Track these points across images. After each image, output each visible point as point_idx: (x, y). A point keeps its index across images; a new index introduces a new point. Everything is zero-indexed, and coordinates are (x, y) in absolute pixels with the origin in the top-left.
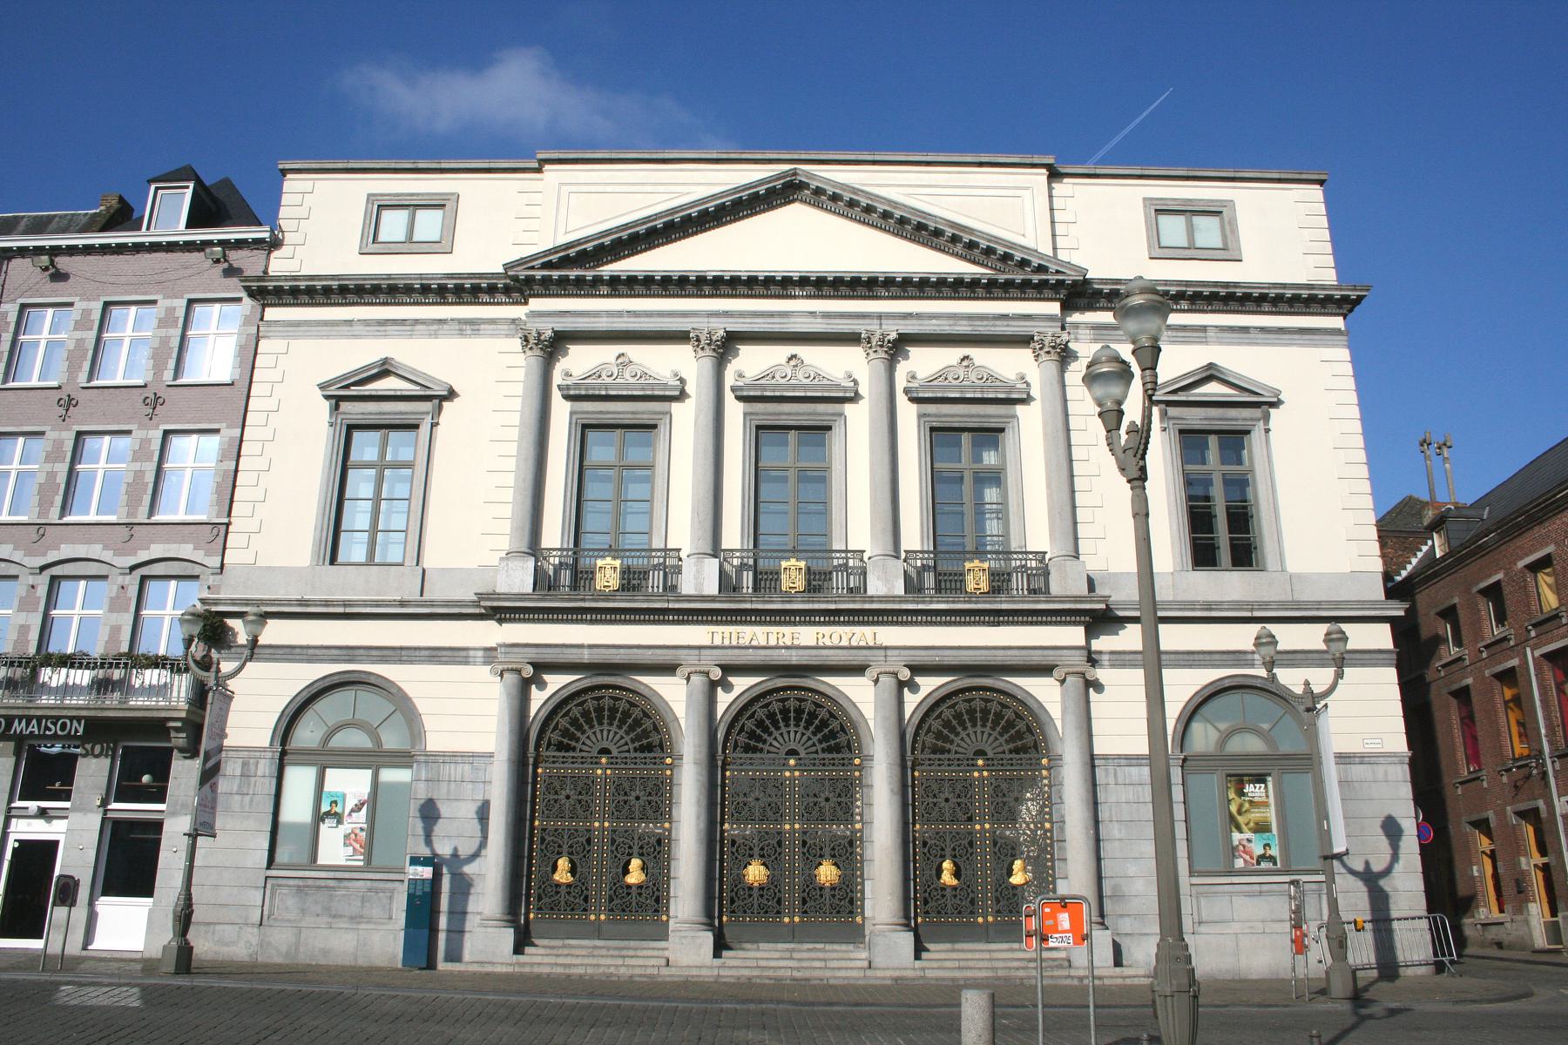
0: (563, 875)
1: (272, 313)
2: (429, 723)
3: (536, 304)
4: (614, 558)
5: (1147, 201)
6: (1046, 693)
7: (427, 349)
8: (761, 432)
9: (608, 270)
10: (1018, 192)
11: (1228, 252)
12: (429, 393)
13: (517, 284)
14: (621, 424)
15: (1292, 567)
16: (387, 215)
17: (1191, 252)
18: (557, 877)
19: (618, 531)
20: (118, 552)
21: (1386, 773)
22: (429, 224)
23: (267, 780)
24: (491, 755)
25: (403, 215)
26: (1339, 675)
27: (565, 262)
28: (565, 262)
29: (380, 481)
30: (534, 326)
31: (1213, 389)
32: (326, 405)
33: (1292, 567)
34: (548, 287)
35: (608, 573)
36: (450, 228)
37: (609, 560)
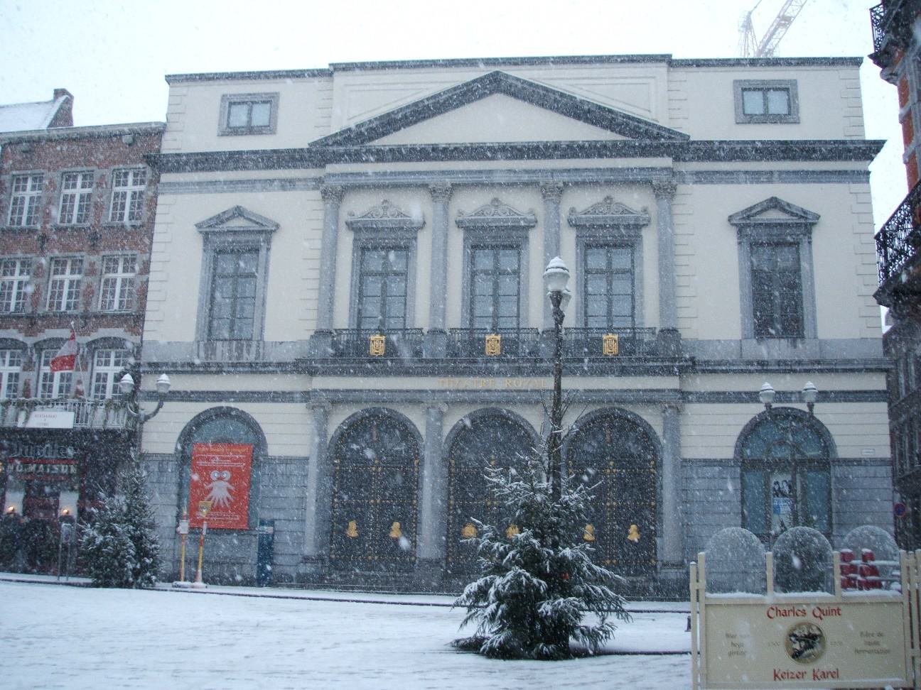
0: (634, 536)
1: (165, 178)
2: (837, 440)
3: (331, 168)
4: (381, 335)
5: (224, 97)
6: (652, 417)
7: (265, 203)
8: (362, 249)
9: (378, 143)
10: (645, 81)
11: (790, 116)
12: (263, 228)
13: (319, 154)
14: (383, 244)
15: (822, 335)
16: (235, 109)
17: (767, 118)
18: (629, 537)
19: (496, 316)
20: (28, 334)
21: (875, 472)
22: (240, 117)
23: (174, 475)
24: (307, 459)
25: (245, 108)
26: (160, 406)
27: (348, 140)
28: (348, 140)
29: (610, 283)
30: (331, 182)
31: (774, 216)
32: (734, 231)
33: (822, 335)
34: (337, 158)
35: (493, 344)
36: (273, 116)
37: (610, 335)
